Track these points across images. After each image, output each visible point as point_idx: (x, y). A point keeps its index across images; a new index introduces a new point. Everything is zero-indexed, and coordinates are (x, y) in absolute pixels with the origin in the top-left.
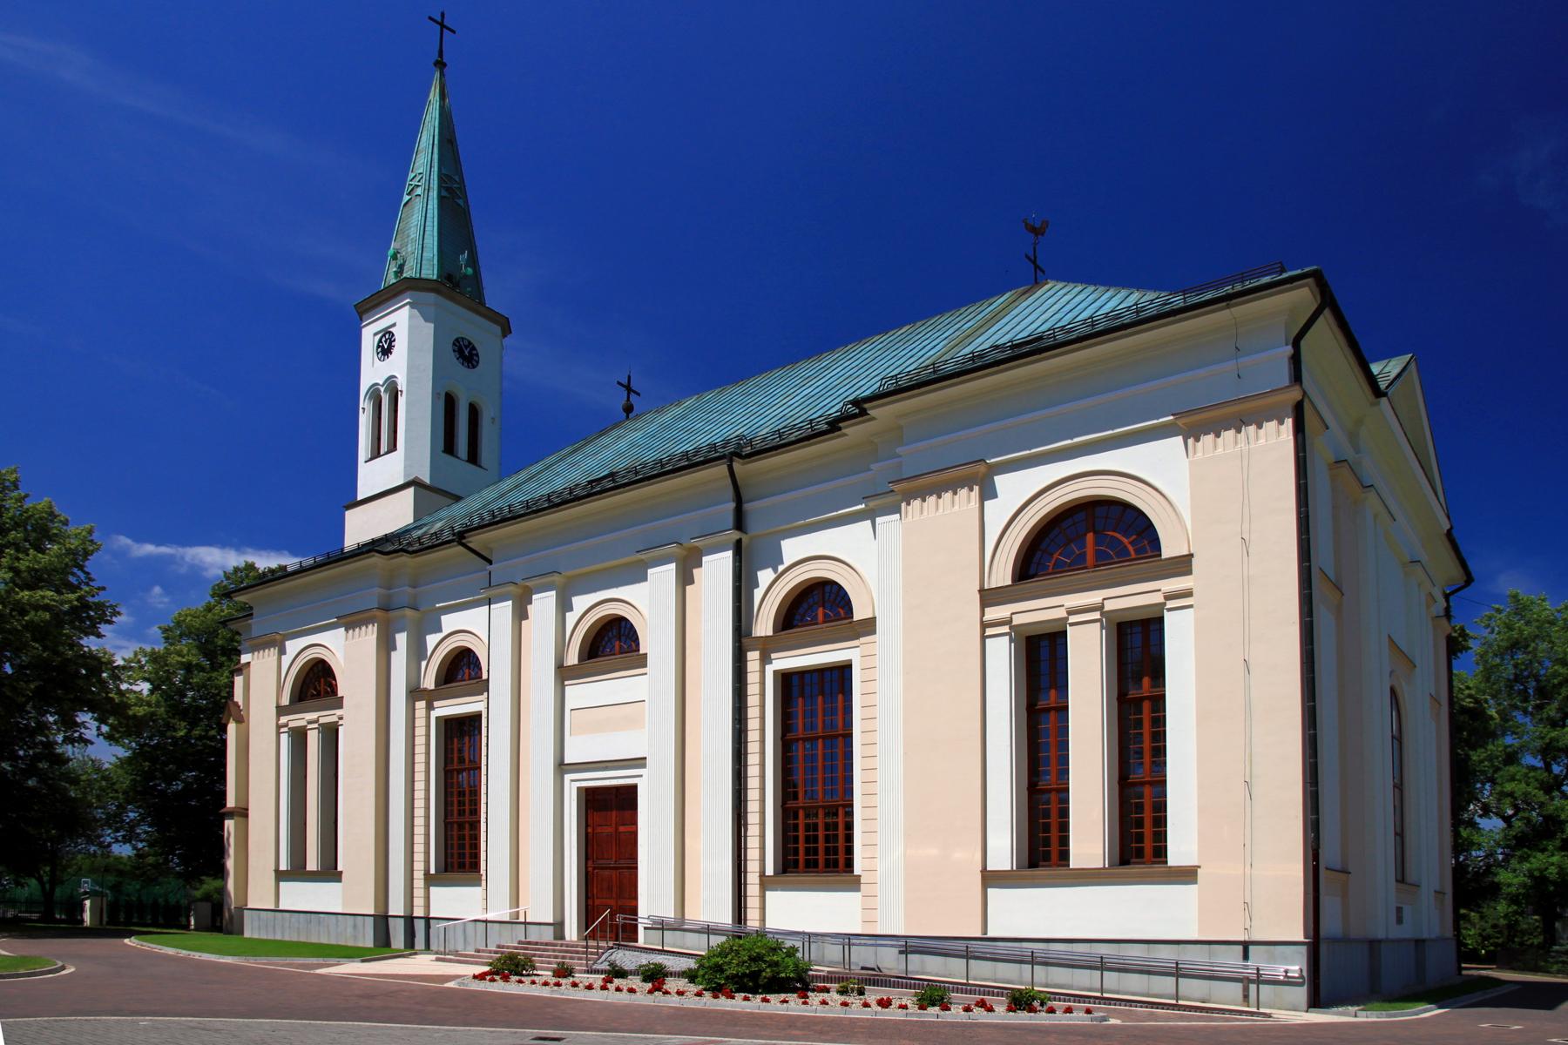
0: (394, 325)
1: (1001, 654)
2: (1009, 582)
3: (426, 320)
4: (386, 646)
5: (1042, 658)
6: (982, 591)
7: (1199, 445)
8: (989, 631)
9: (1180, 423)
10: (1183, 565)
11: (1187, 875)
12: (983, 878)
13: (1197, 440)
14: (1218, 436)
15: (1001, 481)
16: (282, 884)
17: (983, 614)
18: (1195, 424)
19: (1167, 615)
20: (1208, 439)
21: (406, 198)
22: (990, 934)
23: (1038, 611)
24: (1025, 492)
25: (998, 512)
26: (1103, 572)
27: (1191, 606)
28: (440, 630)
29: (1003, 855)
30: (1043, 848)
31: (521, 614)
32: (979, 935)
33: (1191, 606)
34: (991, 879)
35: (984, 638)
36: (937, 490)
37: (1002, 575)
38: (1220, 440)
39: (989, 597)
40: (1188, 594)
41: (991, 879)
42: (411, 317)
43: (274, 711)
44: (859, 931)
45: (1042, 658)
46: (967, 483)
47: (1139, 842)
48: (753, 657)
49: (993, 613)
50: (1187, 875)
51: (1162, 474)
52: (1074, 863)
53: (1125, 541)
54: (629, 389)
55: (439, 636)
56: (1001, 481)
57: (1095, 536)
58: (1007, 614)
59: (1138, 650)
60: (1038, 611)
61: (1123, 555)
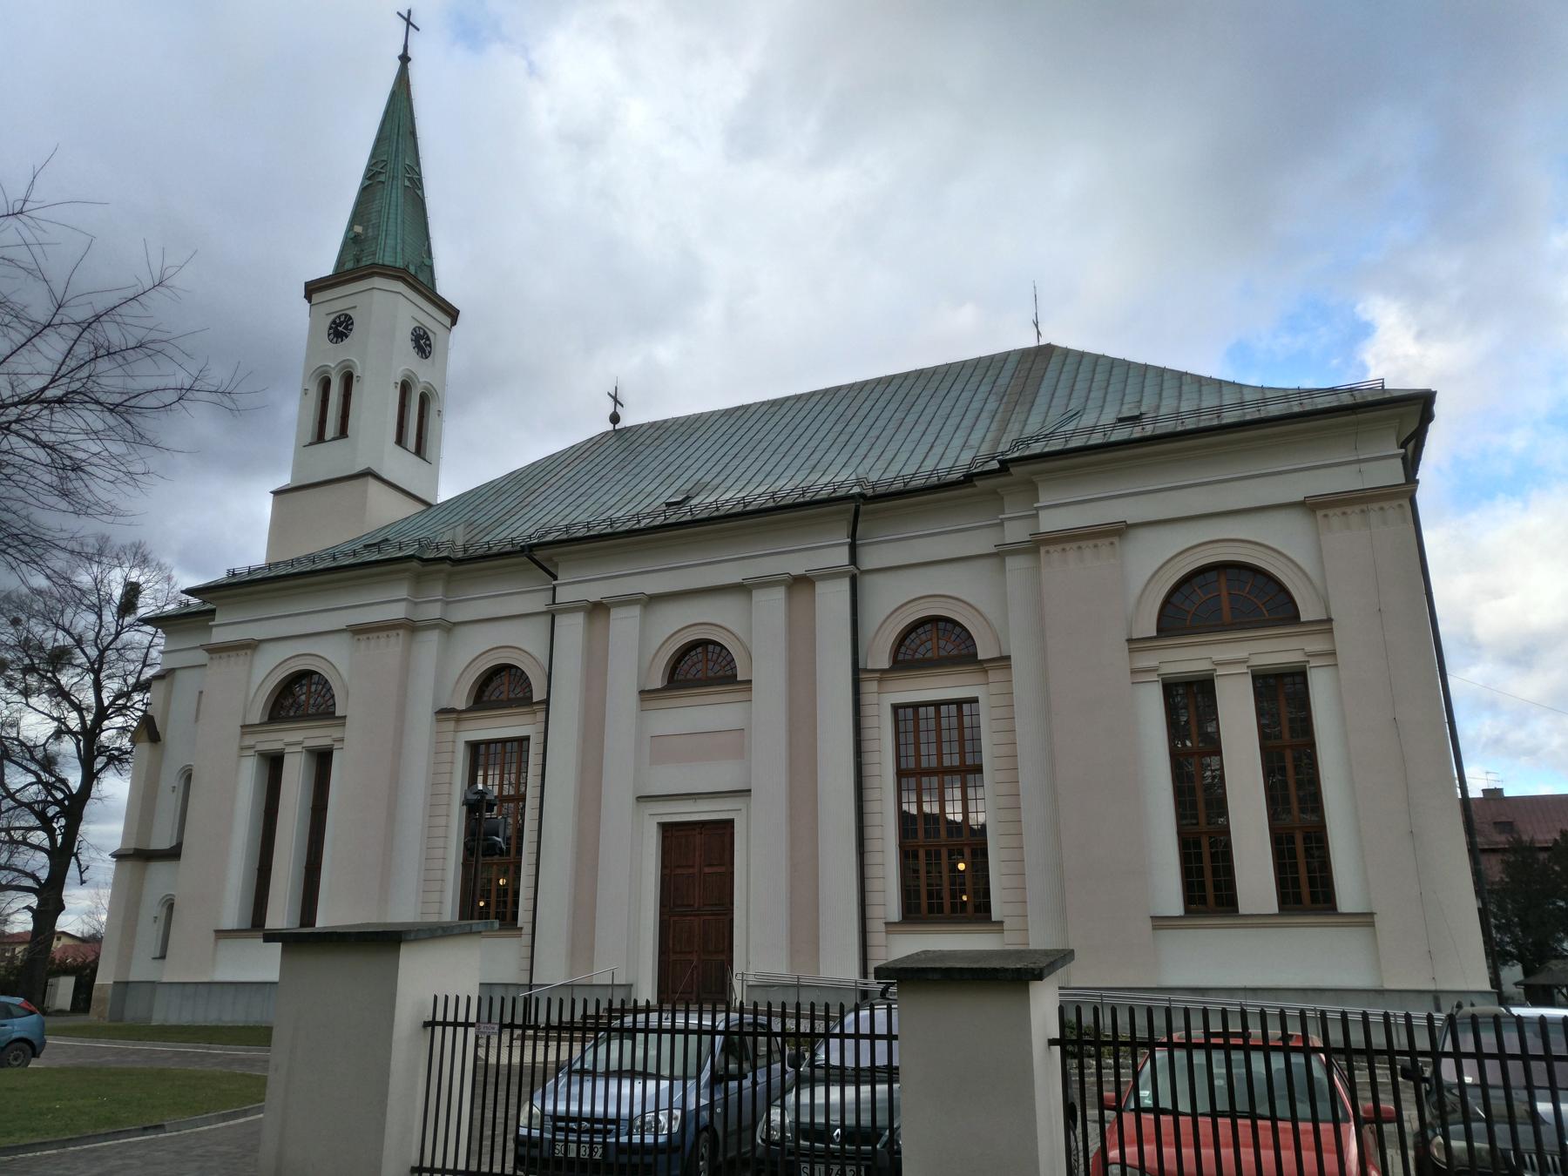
41: (1161, 922)
48: (870, 687)
54: (616, 401)
57: (300, 696)
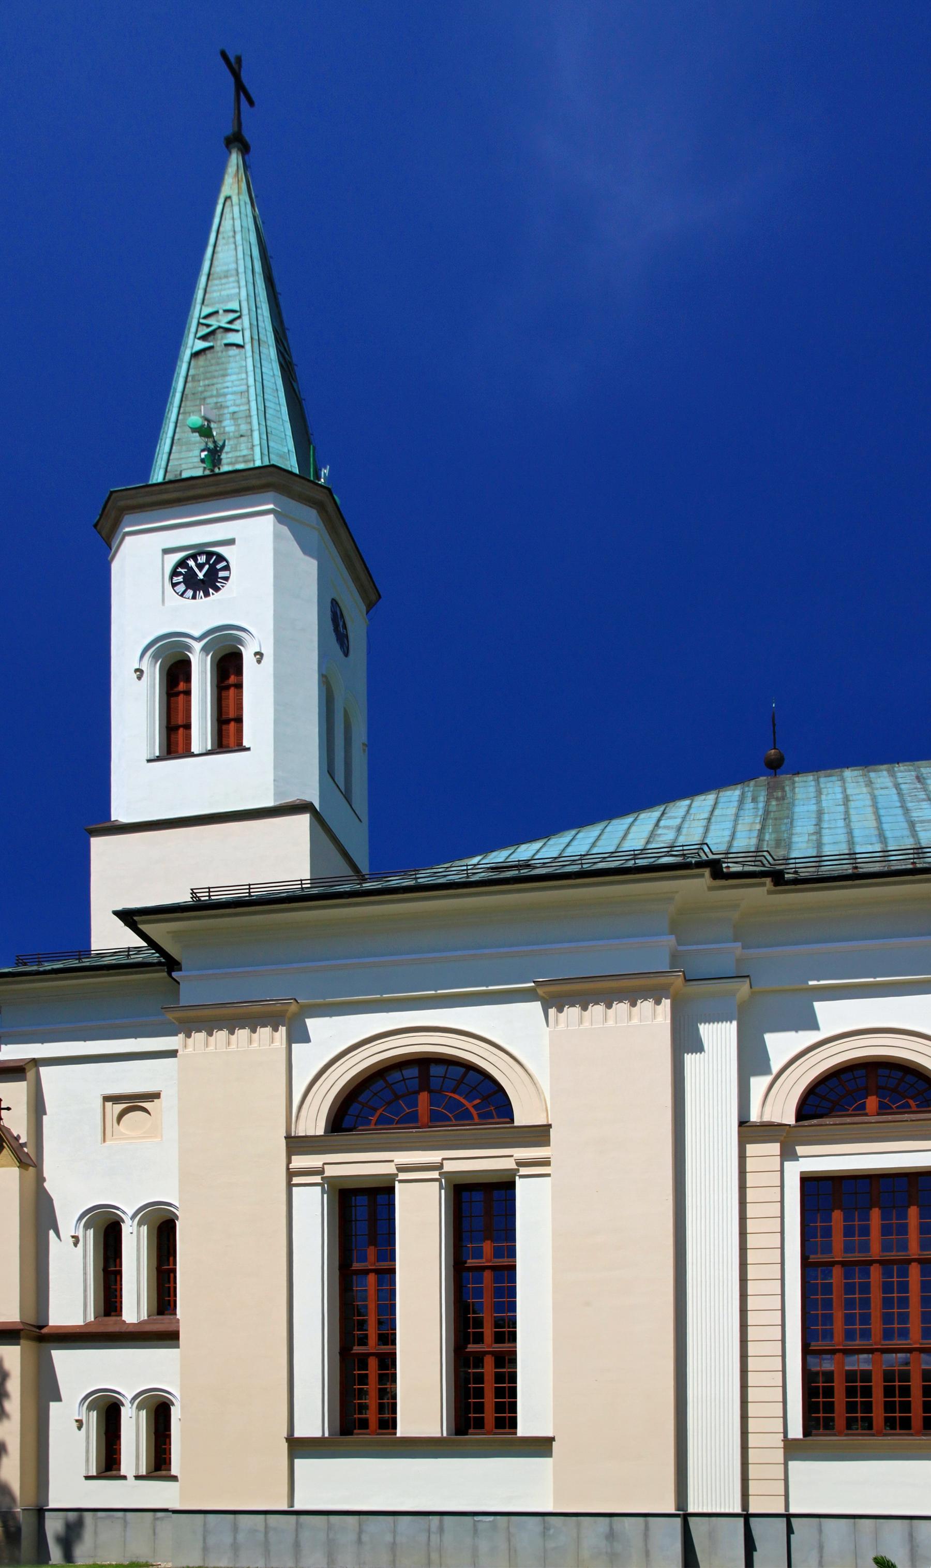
0: (231, 542)
1: (312, 1207)
2: (320, 1131)
3: (306, 551)
4: (685, 1041)
5: (361, 1220)
6: (288, 1138)
7: (562, 1016)
8: (296, 1180)
9: (540, 991)
10: (539, 1135)
11: (541, 1446)
12: (786, 1448)
13: (560, 1010)
14: (210, 1034)
15: (313, 1024)
16: (297, 1462)
17: (289, 1161)
18: (559, 994)
19: (519, 1182)
20: (572, 1012)
21: (192, 344)
22: (297, 1507)
23: (359, 1164)
24: (343, 1042)
25: (308, 1058)
26: (440, 1131)
27: (548, 1175)
28: (815, 1026)
29: (313, 1421)
30: (362, 1411)
31: (685, 1041)
32: (285, 1507)
33: (548, 1175)
34: (299, 1447)
35: (290, 1186)
36: (232, 1023)
37: (313, 1122)
38: (212, 1039)
39: (296, 1144)
40: (546, 1163)
41: (299, 1447)
42: (277, 536)
43: (283, 1143)
44: (550, 1509)
45: (361, 1220)
46: (273, 1020)
47: (483, 1407)
49: (299, 1162)
50: (541, 1446)
51: (511, 1037)
52: (402, 1430)
53: (468, 1105)
55: (808, 1038)
56: (313, 1024)
57: (456, 1095)
58: (439, 1159)
59: (482, 1217)
60: (359, 1164)
61: (464, 1116)
